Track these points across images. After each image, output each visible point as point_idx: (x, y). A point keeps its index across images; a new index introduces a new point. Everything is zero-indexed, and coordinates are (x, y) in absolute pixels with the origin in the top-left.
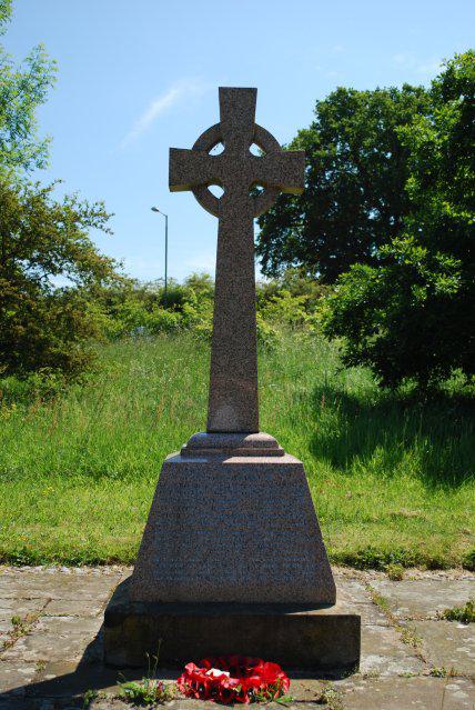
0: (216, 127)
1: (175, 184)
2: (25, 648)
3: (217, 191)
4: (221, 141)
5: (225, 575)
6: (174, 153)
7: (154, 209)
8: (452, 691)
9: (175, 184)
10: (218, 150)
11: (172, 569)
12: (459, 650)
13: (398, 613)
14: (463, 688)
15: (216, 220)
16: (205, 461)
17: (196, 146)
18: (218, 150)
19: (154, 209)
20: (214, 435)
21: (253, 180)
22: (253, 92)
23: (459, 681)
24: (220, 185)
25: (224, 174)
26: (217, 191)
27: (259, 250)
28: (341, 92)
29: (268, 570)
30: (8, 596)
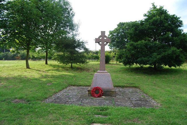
10: (101, 38)
18: (101, 38)
26: (101, 43)
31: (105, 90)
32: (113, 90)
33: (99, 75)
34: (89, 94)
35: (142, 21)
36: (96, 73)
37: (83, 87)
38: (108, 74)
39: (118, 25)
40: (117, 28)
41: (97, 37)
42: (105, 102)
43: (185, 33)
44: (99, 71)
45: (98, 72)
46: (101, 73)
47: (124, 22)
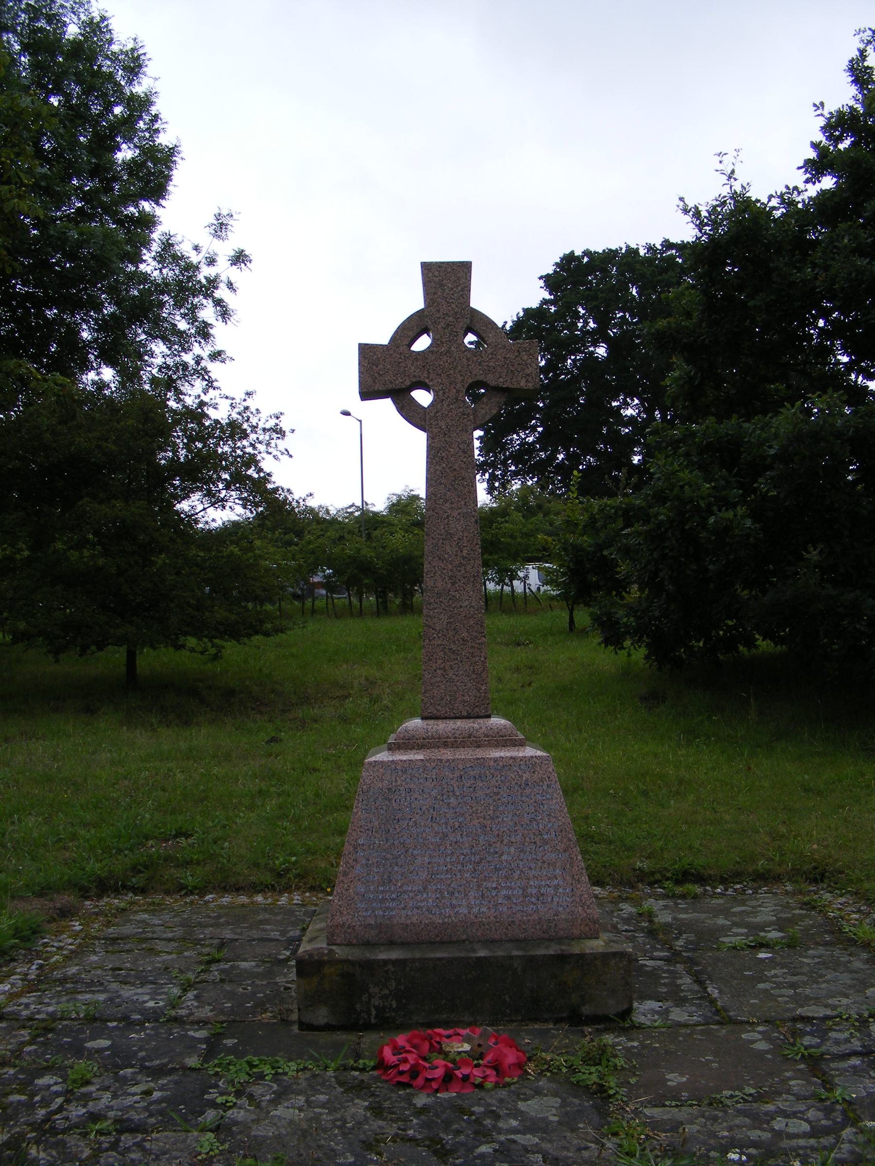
0: (419, 314)
1: (367, 394)
2: (196, 1004)
3: (423, 398)
4: (425, 331)
5: (453, 906)
6: (366, 352)
7: (346, 413)
8: (753, 1042)
9: (367, 394)
10: (423, 343)
11: (384, 900)
12: (761, 986)
13: (680, 942)
14: (766, 1036)
15: (385, 341)
16: (421, 757)
17: (393, 339)
18: (423, 343)
19: (346, 413)
20: (431, 722)
21: (470, 381)
22: (360, 345)
23: (760, 1028)
24: (427, 388)
25: (432, 376)
26: (423, 398)
27: (482, 467)
28: (569, 259)
29: (508, 898)
30: (170, 935)
31: (490, 943)
32: (597, 945)
33: (406, 768)
34: (309, 1001)
35: (688, 243)
36: (383, 756)
37: (243, 899)
38: (529, 752)
39: (550, 282)
40: (545, 302)
41: (383, 337)
42: (516, 1113)
43: (642, 252)
44: (415, 723)
45: (408, 743)
46: (447, 754)
47: (598, 247)
